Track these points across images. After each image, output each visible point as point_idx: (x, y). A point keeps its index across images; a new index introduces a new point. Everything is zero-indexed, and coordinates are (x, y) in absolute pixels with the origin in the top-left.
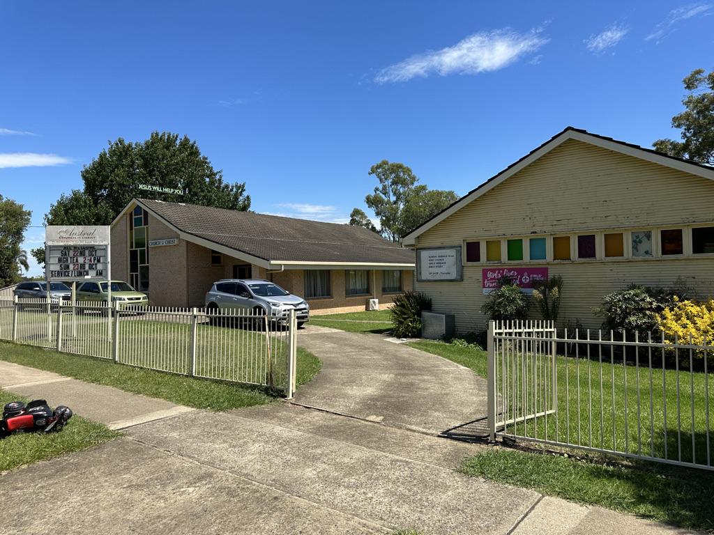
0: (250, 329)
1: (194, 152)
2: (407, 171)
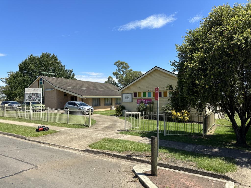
0: (78, 115)
1: (56, 59)
2: (126, 64)
